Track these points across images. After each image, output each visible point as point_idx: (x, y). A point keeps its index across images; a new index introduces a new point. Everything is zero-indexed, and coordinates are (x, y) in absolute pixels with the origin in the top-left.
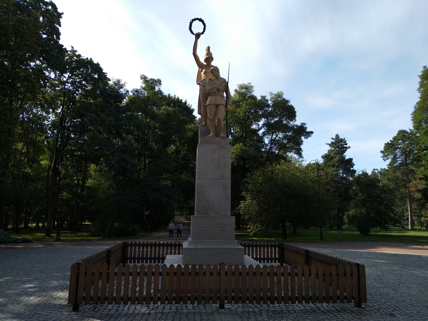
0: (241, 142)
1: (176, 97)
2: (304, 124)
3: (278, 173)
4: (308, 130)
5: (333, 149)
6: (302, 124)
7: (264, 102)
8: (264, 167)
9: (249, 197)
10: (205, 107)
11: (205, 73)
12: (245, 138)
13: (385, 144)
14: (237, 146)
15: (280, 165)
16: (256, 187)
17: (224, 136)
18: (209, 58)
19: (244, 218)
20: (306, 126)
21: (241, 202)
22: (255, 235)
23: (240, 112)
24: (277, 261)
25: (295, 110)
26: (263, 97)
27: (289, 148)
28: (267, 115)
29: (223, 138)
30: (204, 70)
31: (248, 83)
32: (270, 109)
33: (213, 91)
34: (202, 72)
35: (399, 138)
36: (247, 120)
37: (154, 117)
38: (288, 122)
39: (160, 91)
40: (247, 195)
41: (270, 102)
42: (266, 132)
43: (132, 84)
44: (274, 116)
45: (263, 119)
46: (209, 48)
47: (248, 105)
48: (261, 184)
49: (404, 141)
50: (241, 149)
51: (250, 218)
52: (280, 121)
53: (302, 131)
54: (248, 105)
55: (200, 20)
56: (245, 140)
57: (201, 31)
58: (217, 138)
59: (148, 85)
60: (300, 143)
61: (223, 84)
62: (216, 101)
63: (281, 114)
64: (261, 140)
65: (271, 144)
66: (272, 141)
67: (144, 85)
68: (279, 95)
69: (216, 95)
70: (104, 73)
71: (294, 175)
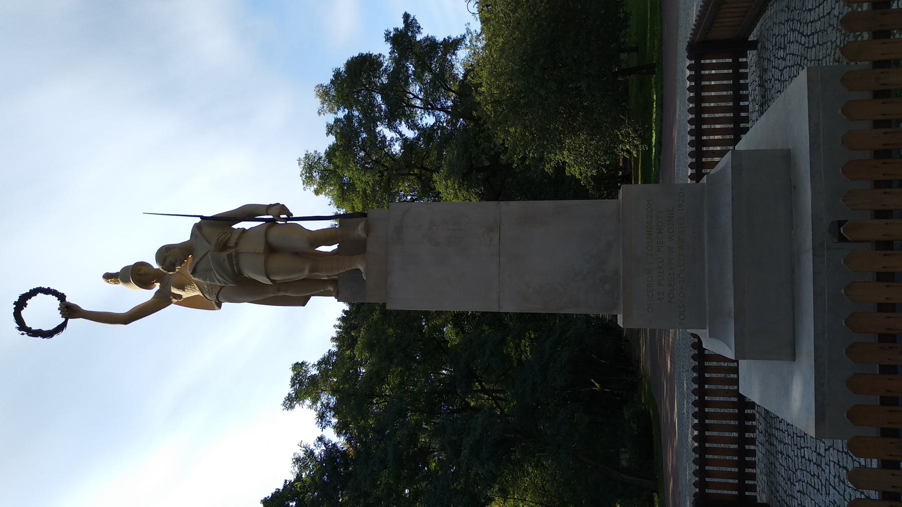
0: (430, 179)
1: (338, 323)
2: (387, 34)
3: (498, 87)
4: (401, 26)
6: (387, 40)
7: (342, 129)
8: (485, 123)
9: (556, 154)
10: (287, 285)
11: (182, 288)
12: (422, 168)
14: (440, 187)
15: (481, 85)
16: (534, 141)
17: (361, 226)
18: (137, 274)
19: (605, 166)
20: (392, 30)
21: (567, 174)
22: (646, 140)
23: (364, 181)
24: (741, 60)
25: (357, 55)
26: (330, 130)
27: (442, 67)
28: (370, 121)
29: (368, 229)
30: (174, 291)
31: (299, 164)
32: (356, 113)
33: (227, 263)
34: (180, 296)
36: (383, 165)
37: (377, 377)
38: (386, 70)
39: (319, 363)
40: (551, 160)
41: (341, 115)
42: (407, 122)
43: (309, 428)
44: (373, 104)
45: (378, 129)
46: (108, 277)
47: (347, 163)
48: (525, 127)
50: (446, 178)
51: (606, 153)
52: (383, 90)
53: (404, 39)
54: (347, 163)
55: (21, 304)
56: (427, 170)
57: (54, 302)
58: (369, 248)
59: (306, 394)
60: (431, 43)
61: (207, 230)
62: (258, 253)
63: (367, 89)
64: (426, 133)
65: (434, 108)
66: (429, 107)
67: (308, 402)
68: (323, 93)
69: (238, 254)
70: (285, 486)
71: (502, 50)
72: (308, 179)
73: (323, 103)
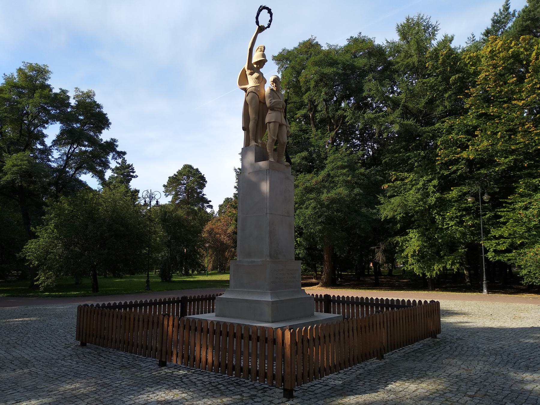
4: (118, 149)
5: (116, 175)
13: (169, 178)
33: (279, 106)
35: (184, 173)
41: (73, 102)
49: (188, 177)
55: (270, 11)
68: (89, 95)
72: (32, 68)
73: (82, 92)
